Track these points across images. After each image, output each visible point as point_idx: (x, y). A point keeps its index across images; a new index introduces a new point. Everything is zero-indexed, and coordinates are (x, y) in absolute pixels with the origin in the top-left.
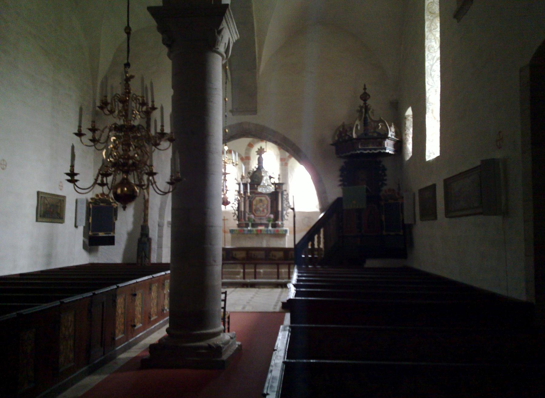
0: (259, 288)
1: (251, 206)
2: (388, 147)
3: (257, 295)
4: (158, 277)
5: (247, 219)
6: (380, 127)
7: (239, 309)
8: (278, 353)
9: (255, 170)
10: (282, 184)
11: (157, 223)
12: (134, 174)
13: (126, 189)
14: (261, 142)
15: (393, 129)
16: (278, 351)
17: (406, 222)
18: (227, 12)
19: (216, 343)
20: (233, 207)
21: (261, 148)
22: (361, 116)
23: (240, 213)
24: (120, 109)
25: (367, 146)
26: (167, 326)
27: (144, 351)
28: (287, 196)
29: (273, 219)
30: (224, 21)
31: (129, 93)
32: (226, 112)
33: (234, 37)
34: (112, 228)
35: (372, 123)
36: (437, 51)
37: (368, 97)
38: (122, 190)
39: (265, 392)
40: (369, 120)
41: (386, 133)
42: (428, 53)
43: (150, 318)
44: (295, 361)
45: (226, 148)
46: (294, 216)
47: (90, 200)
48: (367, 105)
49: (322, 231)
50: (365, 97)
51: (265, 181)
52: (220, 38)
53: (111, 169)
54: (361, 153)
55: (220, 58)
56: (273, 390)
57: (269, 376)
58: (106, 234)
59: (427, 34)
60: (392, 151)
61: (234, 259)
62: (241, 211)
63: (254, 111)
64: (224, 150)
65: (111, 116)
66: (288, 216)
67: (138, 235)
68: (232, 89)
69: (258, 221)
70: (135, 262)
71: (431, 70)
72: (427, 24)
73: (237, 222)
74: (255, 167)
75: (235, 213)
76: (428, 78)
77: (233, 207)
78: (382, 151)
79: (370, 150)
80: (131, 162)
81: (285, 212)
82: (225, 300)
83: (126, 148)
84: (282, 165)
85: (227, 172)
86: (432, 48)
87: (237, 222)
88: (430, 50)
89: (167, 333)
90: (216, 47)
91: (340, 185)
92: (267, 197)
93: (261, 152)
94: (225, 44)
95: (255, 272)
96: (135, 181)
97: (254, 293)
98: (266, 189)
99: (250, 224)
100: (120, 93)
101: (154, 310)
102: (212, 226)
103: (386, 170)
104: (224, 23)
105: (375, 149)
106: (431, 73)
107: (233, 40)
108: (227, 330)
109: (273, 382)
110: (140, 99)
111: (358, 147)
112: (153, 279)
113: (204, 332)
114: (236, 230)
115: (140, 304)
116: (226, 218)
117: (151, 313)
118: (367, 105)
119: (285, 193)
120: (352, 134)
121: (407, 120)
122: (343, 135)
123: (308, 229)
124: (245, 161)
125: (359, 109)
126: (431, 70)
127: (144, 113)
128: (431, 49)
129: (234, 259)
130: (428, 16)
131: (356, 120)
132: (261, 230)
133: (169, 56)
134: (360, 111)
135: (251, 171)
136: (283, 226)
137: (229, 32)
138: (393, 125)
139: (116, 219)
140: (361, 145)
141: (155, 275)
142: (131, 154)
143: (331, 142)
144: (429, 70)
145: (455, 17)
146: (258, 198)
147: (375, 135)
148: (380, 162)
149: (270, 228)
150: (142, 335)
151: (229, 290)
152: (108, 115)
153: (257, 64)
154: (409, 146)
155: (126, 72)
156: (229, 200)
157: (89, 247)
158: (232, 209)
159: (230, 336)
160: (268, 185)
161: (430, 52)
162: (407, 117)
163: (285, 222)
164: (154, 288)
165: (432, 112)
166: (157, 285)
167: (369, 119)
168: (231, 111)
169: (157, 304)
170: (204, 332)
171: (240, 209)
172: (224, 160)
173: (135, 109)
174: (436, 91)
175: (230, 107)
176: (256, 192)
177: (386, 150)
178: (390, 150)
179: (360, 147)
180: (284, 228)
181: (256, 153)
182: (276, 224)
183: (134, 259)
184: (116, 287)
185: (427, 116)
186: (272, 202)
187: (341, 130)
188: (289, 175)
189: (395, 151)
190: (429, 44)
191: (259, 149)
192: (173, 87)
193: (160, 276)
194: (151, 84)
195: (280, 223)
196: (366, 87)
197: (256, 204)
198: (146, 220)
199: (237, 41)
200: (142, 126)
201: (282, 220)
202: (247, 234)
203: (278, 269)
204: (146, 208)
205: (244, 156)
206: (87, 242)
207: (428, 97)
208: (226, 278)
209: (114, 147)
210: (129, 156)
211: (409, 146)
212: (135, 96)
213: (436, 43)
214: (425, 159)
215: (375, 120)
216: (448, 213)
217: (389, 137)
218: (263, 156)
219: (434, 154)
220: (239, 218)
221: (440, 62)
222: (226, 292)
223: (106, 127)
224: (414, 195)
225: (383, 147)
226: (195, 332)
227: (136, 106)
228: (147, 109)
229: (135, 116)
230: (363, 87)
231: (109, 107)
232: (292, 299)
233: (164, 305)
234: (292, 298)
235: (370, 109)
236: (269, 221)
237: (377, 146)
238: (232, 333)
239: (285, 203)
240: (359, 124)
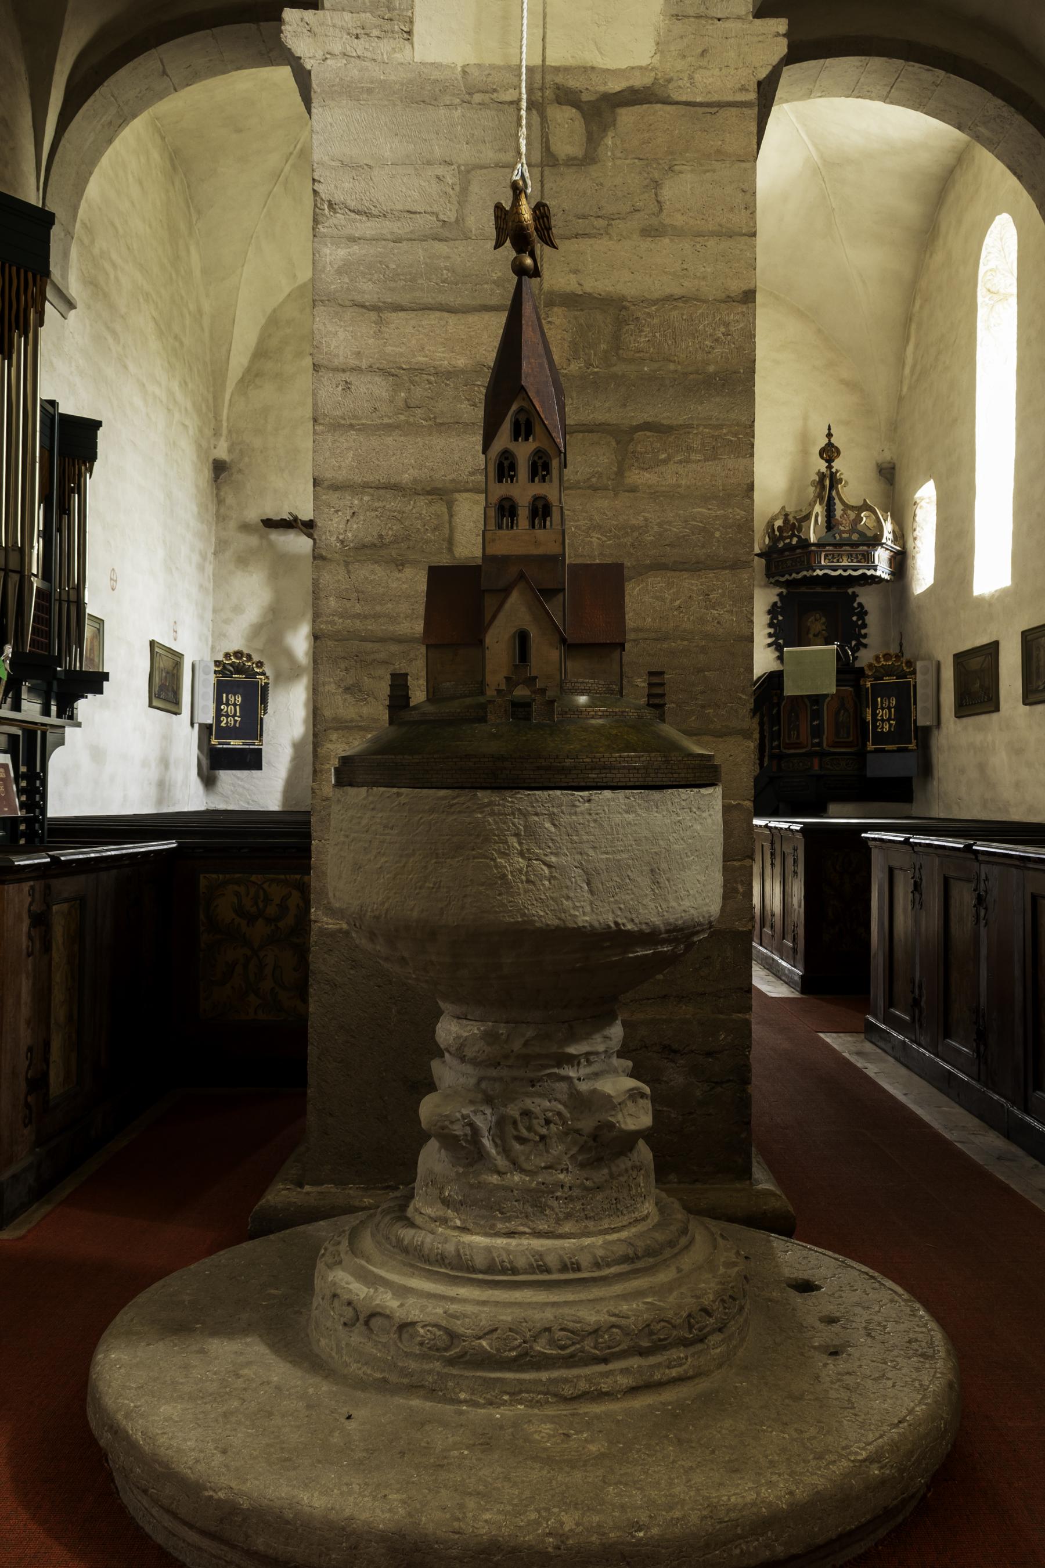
25: (838, 561)
48: (834, 470)
50: (829, 452)
78: (869, 573)
103: (866, 613)
118: (834, 470)
147: (855, 537)
148: (855, 596)
167: (837, 501)
189: (892, 574)
206: (205, 762)
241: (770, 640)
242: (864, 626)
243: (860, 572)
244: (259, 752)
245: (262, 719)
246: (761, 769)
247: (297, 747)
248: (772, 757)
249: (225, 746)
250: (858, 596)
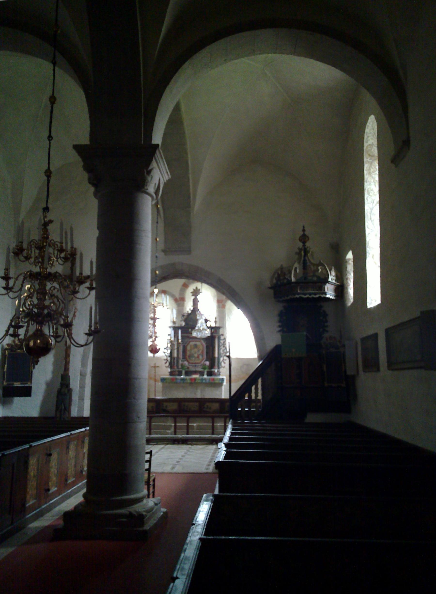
0: (192, 445)
1: (184, 351)
2: (328, 292)
3: (189, 453)
4: (76, 433)
5: (180, 367)
6: (320, 270)
7: (167, 469)
8: (196, 528)
9: (190, 312)
10: (218, 328)
11: (79, 372)
12: (49, 324)
13: (39, 341)
14: (197, 282)
15: (333, 273)
16: (197, 526)
17: (349, 373)
18: (157, 152)
19: (138, 510)
20: (165, 353)
21: (197, 288)
22: (299, 259)
23: (173, 360)
24: (37, 255)
25: (306, 291)
26: (85, 490)
27: (58, 519)
28: (224, 341)
29: (209, 366)
30: (154, 161)
31: (47, 238)
32: (156, 252)
33: (165, 177)
34: (29, 377)
35: (312, 267)
36: (376, 195)
37: (307, 239)
38: (35, 343)
39: (175, 575)
40: (308, 264)
41: (327, 277)
42: (368, 196)
43: (66, 480)
44: (212, 537)
45: (156, 291)
46: (230, 365)
47: (6, 347)
49: (260, 380)
50: (304, 239)
51: (201, 324)
52: (149, 179)
53: (25, 319)
54: (300, 297)
55: (150, 198)
56: (183, 572)
57: (182, 555)
58: (21, 384)
59: (366, 177)
60: (333, 296)
61: (165, 411)
62: (174, 358)
63: (188, 251)
64: (153, 292)
65: (27, 262)
67: (57, 386)
68: (165, 227)
69: (192, 369)
71: (371, 214)
72: (366, 166)
73: (169, 370)
74: (190, 309)
75: (167, 360)
76: (367, 222)
77: (165, 353)
78: (323, 296)
79: (310, 294)
80: (46, 311)
81: (221, 359)
82: (149, 461)
83: (41, 296)
84: (219, 307)
85: (156, 316)
86: (371, 191)
87: (169, 370)
88: (369, 193)
89: (84, 499)
90: (145, 188)
91: (279, 331)
92: (203, 342)
93: (196, 292)
94: (155, 184)
95: (188, 426)
96: (49, 332)
97: (185, 451)
98: (201, 333)
99: (184, 372)
100: (37, 239)
101: (71, 471)
102: (136, 379)
104: (154, 164)
105: (315, 294)
106: (370, 216)
107: (164, 180)
108: (151, 495)
109: (185, 564)
110: (59, 245)
111: (297, 291)
112: (71, 436)
113: (123, 497)
114: (168, 378)
115: (55, 465)
116: (157, 365)
117: (69, 475)
119: (222, 338)
120: (291, 277)
121: (348, 263)
122: (282, 278)
123: (247, 377)
124: (179, 302)
125: (298, 251)
126: (371, 214)
127: (62, 259)
128: (370, 192)
129: (165, 411)
130: (367, 158)
131: (295, 262)
132: (195, 379)
133: (95, 194)
134: (299, 254)
135: (185, 313)
136: (219, 375)
137: (159, 173)
138: (333, 269)
140: (300, 289)
141: (73, 432)
142: (47, 303)
143: (270, 286)
144: (369, 214)
145: (392, 161)
146: (192, 343)
147: (315, 279)
148: (321, 307)
149: (205, 376)
150: (57, 500)
151: (155, 449)
152: (24, 261)
153: (192, 203)
154: (351, 291)
155: (45, 217)
156: (158, 348)
157: (3, 398)
158: (164, 355)
159: (154, 502)
160: (204, 329)
161: (369, 195)
162: (347, 261)
163: (221, 370)
164: (72, 446)
165: (373, 257)
166: (75, 443)
167: (308, 261)
168: (164, 251)
169: (75, 466)
170: (123, 497)
171: (173, 356)
172: (153, 303)
173: (52, 256)
174: (376, 236)
175: (161, 246)
176: (190, 336)
177: (326, 295)
178: (331, 296)
179: (299, 291)
180: (221, 377)
181: (191, 294)
182: (211, 372)
183: (52, 413)
184: (29, 446)
185: (367, 261)
186: (207, 347)
187: (280, 272)
188: (227, 318)
190: (368, 187)
191: (194, 290)
192: (98, 228)
193: (80, 432)
194: (71, 229)
195: (216, 371)
196: (305, 229)
197: (191, 350)
198: (67, 369)
199: (169, 181)
200: (59, 273)
201: (219, 368)
202: (180, 383)
203: (213, 423)
204: (67, 355)
205: (178, 296)
207: (369, 242)
208: (156, 433)
209: (28, 296)
210: (44, 305)
211: (351, 291)
212: (52, 241)
213: (375, 185)
214: (367, 306)
215: (315, 263)
216: (391, 365)
217: (330, 282)
218: (199, 297)
219: (376, 301)
220: (171, 365)
221: (379, 206)
222: (151, 451)
223: (20, 275)
224: (357, 343)
225: (323, 292)
226: (114, 498)
227: (54, 253)
228: (65, 255)
229: (53, 262)
230: (302, 228)
231: (25, 253)
232: (220, 461)
233: (83, 465)
234: (221, 460)
235: (309, 252)
236: (204, 369)
237: (317, 291)
238: (155, 500)
239: (222, 348)
240: (298, 268)
242: (326, 321)
243: (317, 296)
244: (30, 388)
245: (32, 372)
247: (48, 384)
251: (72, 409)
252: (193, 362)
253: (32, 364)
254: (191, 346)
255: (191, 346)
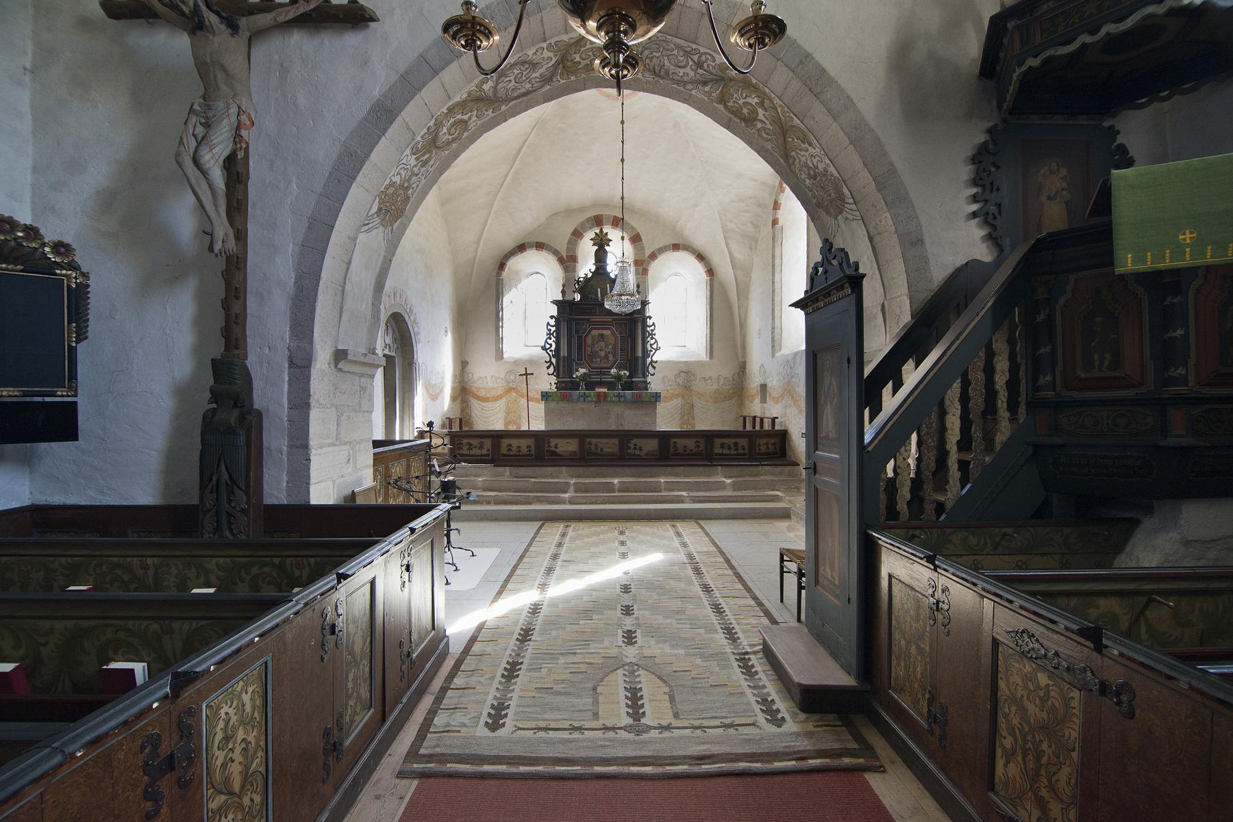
58: (25, 395)
66: (654, 368)
70: (195, 501)
139: (81, 336)
197: (593, 344)
201: (645, 376)
241: (975, 207)
245: (73, 352)
246: (943, 400)
248: (1032, 406)
249: (47, 399)
250: (1118, 132)
251: (266, 478)
252: (597, 366)
253: (70, 323)
254: (593, 338)
255: (593, 338)
